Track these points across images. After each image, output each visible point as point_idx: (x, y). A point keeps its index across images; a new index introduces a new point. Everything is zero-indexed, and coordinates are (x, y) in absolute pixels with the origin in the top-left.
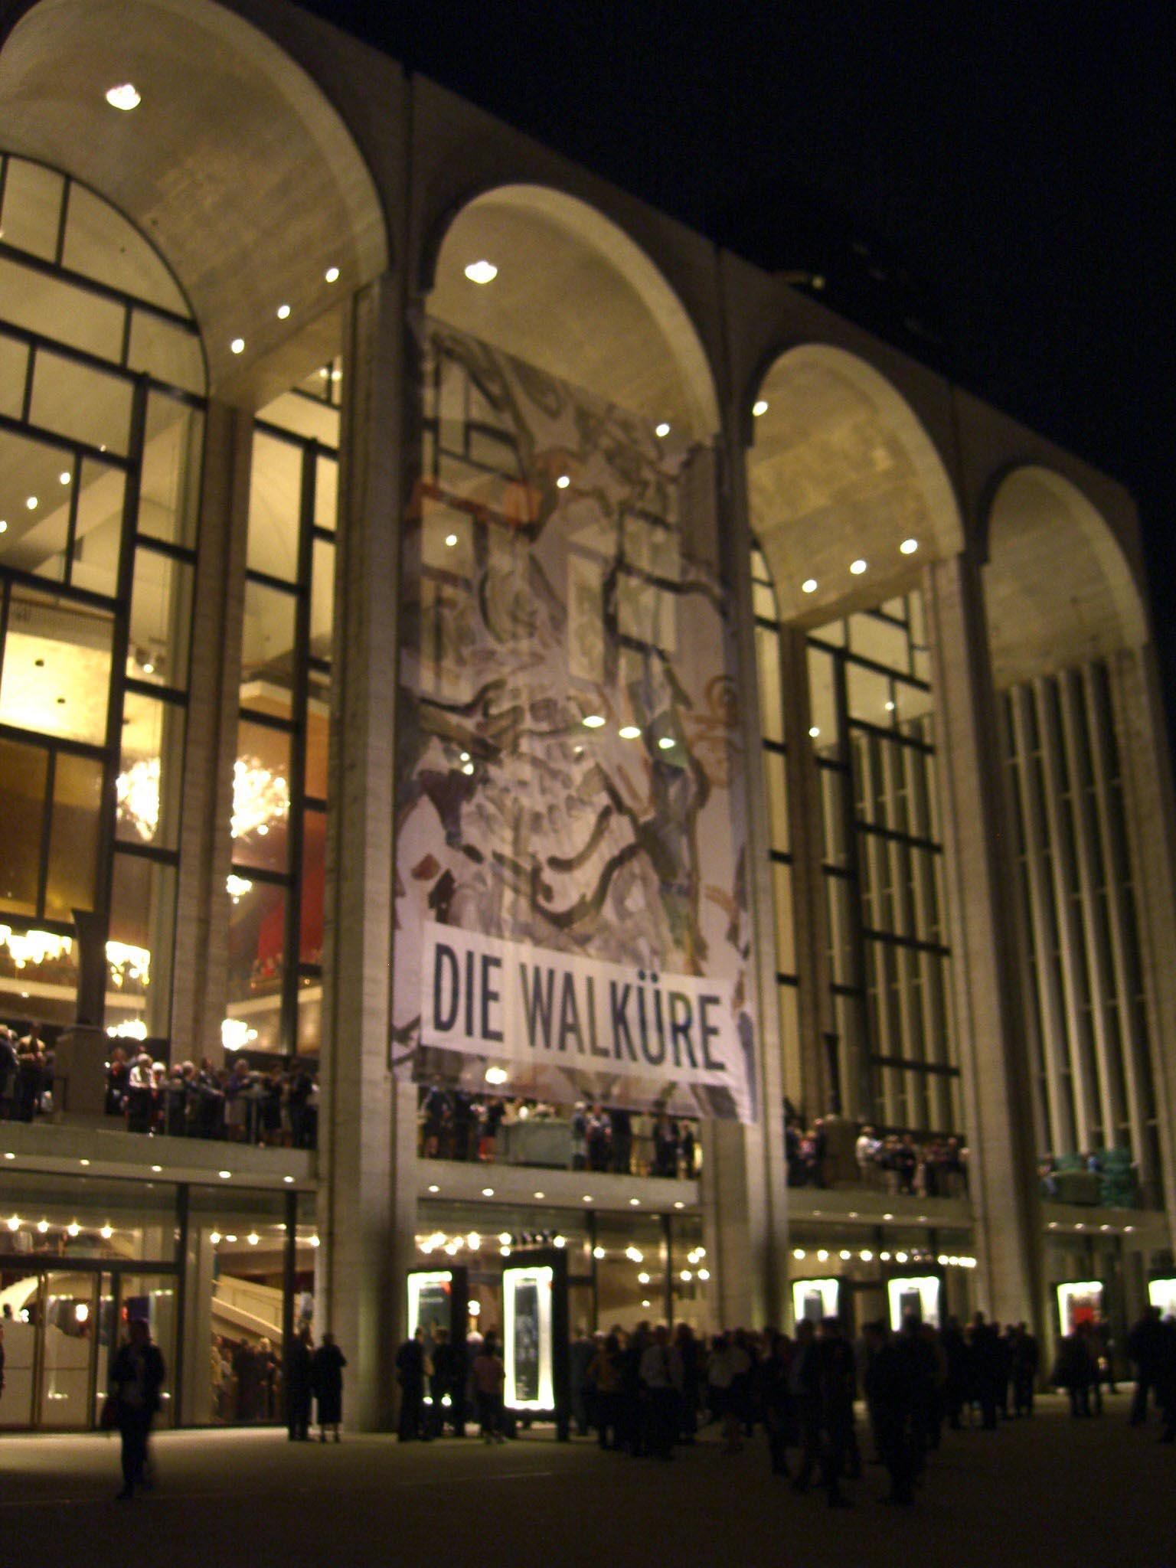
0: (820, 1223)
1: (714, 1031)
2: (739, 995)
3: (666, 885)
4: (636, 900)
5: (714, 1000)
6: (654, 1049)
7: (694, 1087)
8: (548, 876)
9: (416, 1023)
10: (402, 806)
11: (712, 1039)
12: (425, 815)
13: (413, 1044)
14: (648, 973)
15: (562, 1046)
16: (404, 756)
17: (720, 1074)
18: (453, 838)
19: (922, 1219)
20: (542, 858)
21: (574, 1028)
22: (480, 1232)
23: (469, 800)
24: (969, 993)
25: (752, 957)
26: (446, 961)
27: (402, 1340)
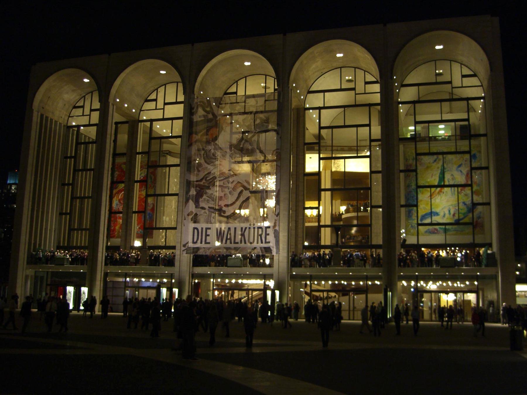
0: (323, 275)
1: (268, 234)
7: (261, 248)
8: (224, 208)
9: (188, 243)
11: (267, 236)
13: (187, 247)
15: (226, 243)
17: (260, 243)
18: (197, 207)
19: (50, 270)
20: (223, 205)
21: (230, 239)
22: (324, 281)
23: (201, 198)
24: (103, 247)
25: (278, 217)
26: (196, 230)
27: (473, 325)
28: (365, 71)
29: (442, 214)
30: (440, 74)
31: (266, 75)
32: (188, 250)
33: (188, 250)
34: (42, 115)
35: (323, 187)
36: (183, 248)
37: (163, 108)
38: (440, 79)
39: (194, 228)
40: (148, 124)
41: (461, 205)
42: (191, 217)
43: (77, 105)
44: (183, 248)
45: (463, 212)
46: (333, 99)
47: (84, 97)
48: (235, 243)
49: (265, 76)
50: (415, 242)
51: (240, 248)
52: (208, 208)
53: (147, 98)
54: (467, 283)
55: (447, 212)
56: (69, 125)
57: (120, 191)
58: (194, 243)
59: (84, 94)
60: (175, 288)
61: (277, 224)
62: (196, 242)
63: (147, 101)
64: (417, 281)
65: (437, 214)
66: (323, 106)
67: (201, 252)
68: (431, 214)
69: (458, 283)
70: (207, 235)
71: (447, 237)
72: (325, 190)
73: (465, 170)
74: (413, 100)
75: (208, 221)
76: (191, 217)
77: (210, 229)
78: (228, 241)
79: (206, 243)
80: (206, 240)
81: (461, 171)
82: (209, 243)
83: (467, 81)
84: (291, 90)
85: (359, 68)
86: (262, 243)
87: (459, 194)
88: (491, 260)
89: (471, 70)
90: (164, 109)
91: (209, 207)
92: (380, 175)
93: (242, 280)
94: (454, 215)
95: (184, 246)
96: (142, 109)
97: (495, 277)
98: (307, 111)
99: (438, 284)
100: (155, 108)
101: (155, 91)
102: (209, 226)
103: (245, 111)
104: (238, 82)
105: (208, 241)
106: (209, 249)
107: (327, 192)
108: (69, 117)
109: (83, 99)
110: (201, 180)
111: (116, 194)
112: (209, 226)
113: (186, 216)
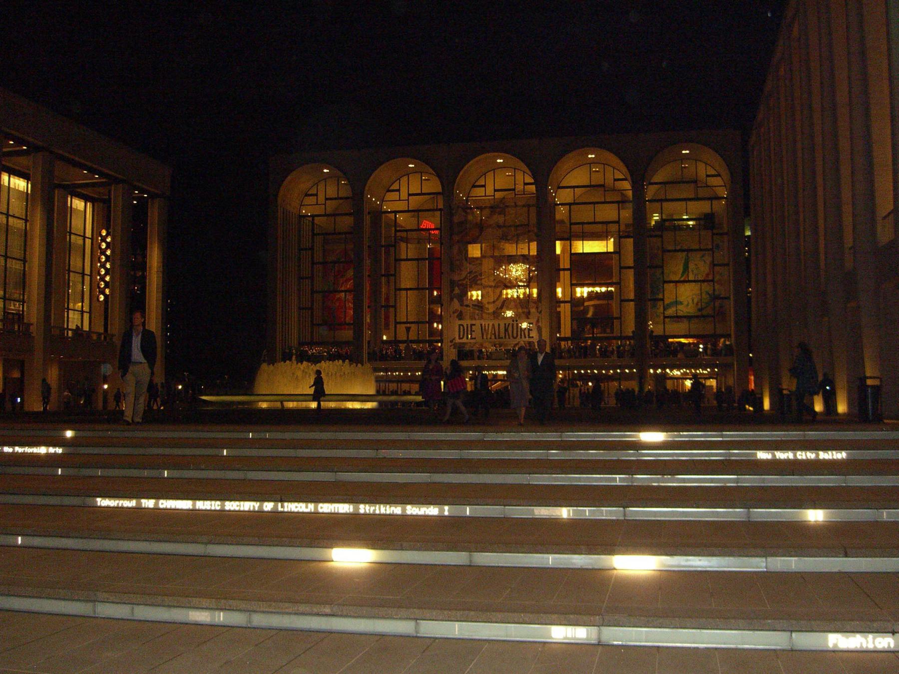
6: (515, 335)
9: (454, 339)
26: (461, 327)
29: (686, 303)
32: (455, 346)
33: (455, 346)
34: (284, 209)
35: (562, 267)
36: (450, 344)
39: (460, 325)
40: (392, 216)
41: (704, 295)
42: (456, 314)
44: (450, 344)
48: (499, 338)
50: (661, 333)
53: (390, 187)
54: (709, 370)
55: (691, 302)
57: (348, 280)
58: (460, 338)
61: (540, 320)
62: (462, 338)
63: (389, 191)
64: (664, 369)
65: (681, 303)
68: (677, 303)
69: (700, 370)
71: (691, 325)
72: (564, 270)
75: (472, 318)
76: (456, 314)
77: (475, 325)
78: (493, 337)
79: (529, 337)
80: (529, 335)
81: (705, 261)
82: (475, 338)
86: (525, 337)
88: (729, 350)
90: (408, 200)
91: (473, 305)
92: (632, 303)
94: (697, 304)
95: (451, 341)
97: (733, 365)
98: (556, 207)
99: (682, 371)
102: (474, 322)
105: (531, 336)
107: (566, 272)
110: (464, 279)
111: (343, 283)
112: (474, 322)
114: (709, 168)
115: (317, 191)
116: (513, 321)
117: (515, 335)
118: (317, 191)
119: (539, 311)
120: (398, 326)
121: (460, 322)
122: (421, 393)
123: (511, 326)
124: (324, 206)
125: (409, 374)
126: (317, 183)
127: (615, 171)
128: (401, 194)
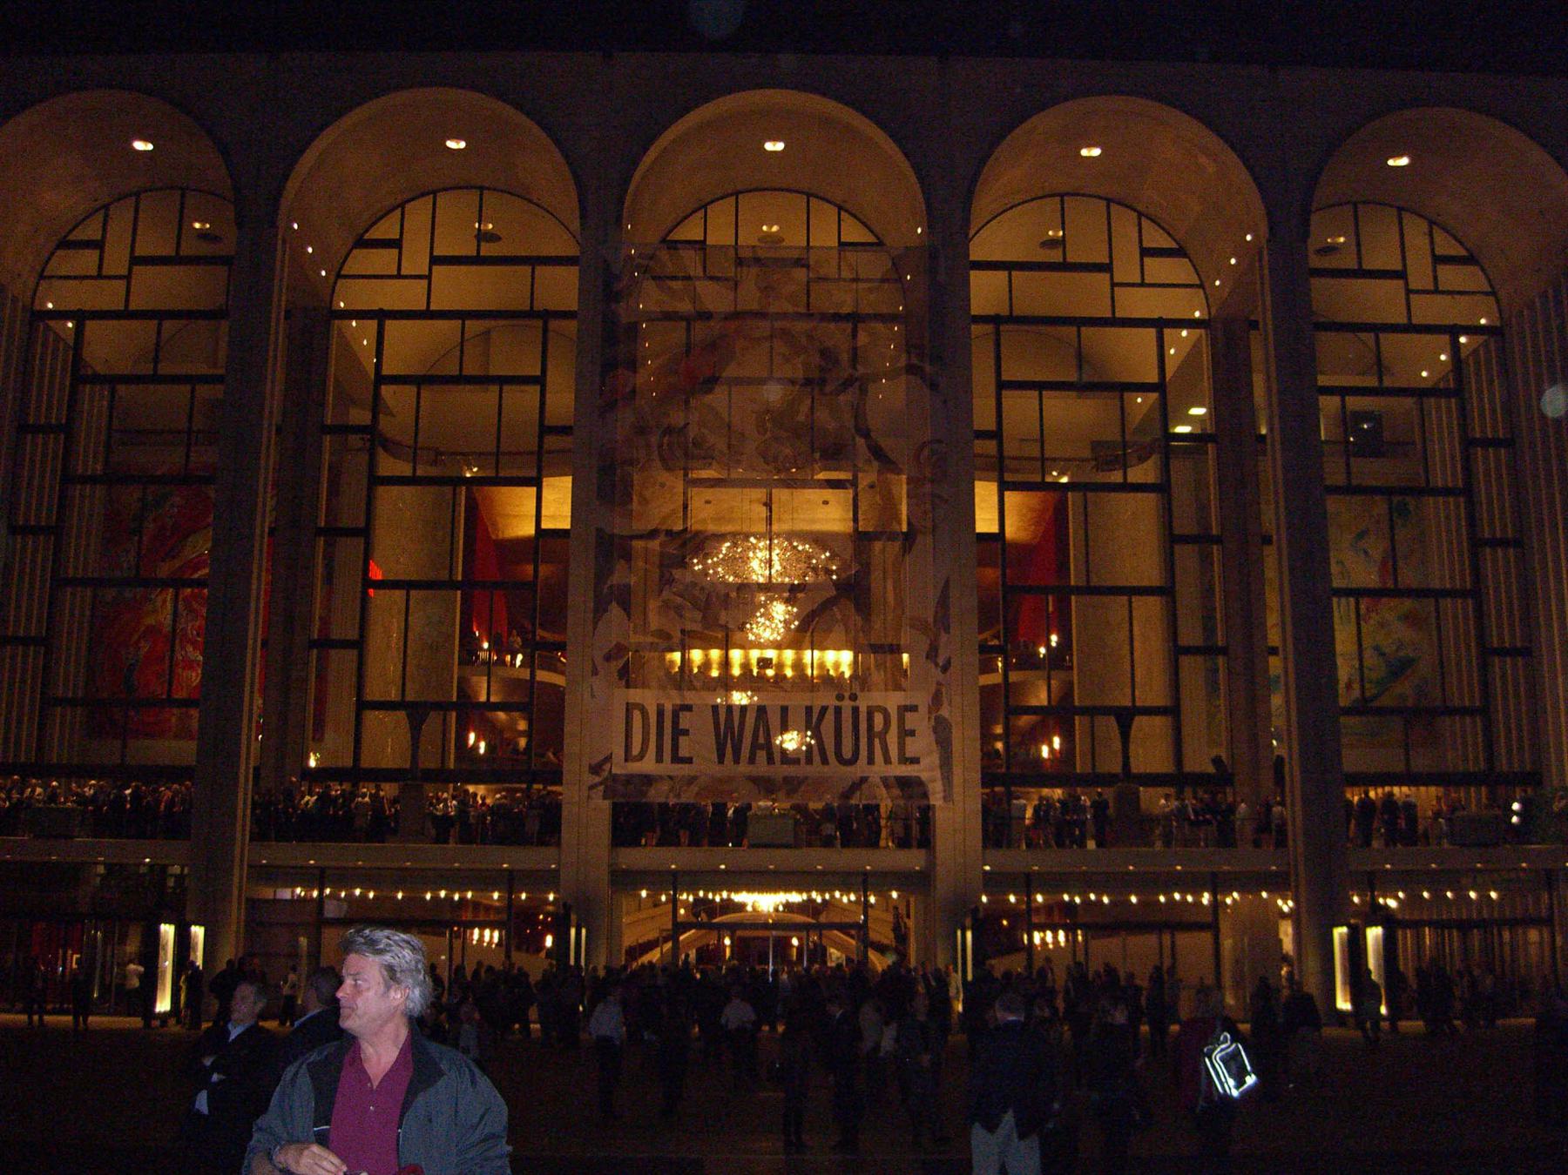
2: (937, 700)
3: (700, 638)
4: (132, 713)
5: (914, 708)
9: (608, 759)
10: (600, 609)
12: (615, 611)
13: (606, 774)
14: (847, 695)
15: (752, 760)
16: (601, 576)
17: (916, 767)
28: (1140, 214)
30: (492, 237)
31: (1109, 201)
32: (613, 786)
33: (613, 786)
37: (1146, 281)
38: (488, 249)
41: (1368, 653)
43: (71, 237)
45: (1374, 676)
46: (455, 287)
47: (106, 207)
49: (1105, 203)
51: (806, 778)
52: (679, 634)
53: (667, 235)
56: (37, 307)
58: (628, 757)
59: (107, 200)
60: (196, 924)
62: (641, 756)
63: (362, 243)
66: (424, 307)
67: (657, 795)
70: (678, 732)
73: (1377, 547)
74: (992, 313)
78: (761, 755)
79: (676, 759)
80: (675, 747)
81: (1366, 553)
82: (689, 761)
83: (1158, 269)
84: (284, 242)
85: (1119, 203)
86: (887, 761)
87: (1362, 623)
89: (872, 232)
90: (429, 277)
93: (730, 891)
95: (595, 769)
96: (343, 273)
100: (1116, 281)
101: (700, 209)
103: (532, 308)
104: (408, 207)
105: (683, 753)
106: (691, 780)
108: (42, 277)
109: (100, 216)
113: (599, 660)
114: (1439, 236)
115: (402, 234)
116: (840, 697)
117: (847, 753)
118: (402, 234)
119: (941, 662)
120: (371, 716)
121: (624, 695)
122: (824, 969)
123: (830, 716)
124: (123, 283)
125: (400, 896)
126: (106, 207)
127: (1145, 222)
128: (106, 255)
